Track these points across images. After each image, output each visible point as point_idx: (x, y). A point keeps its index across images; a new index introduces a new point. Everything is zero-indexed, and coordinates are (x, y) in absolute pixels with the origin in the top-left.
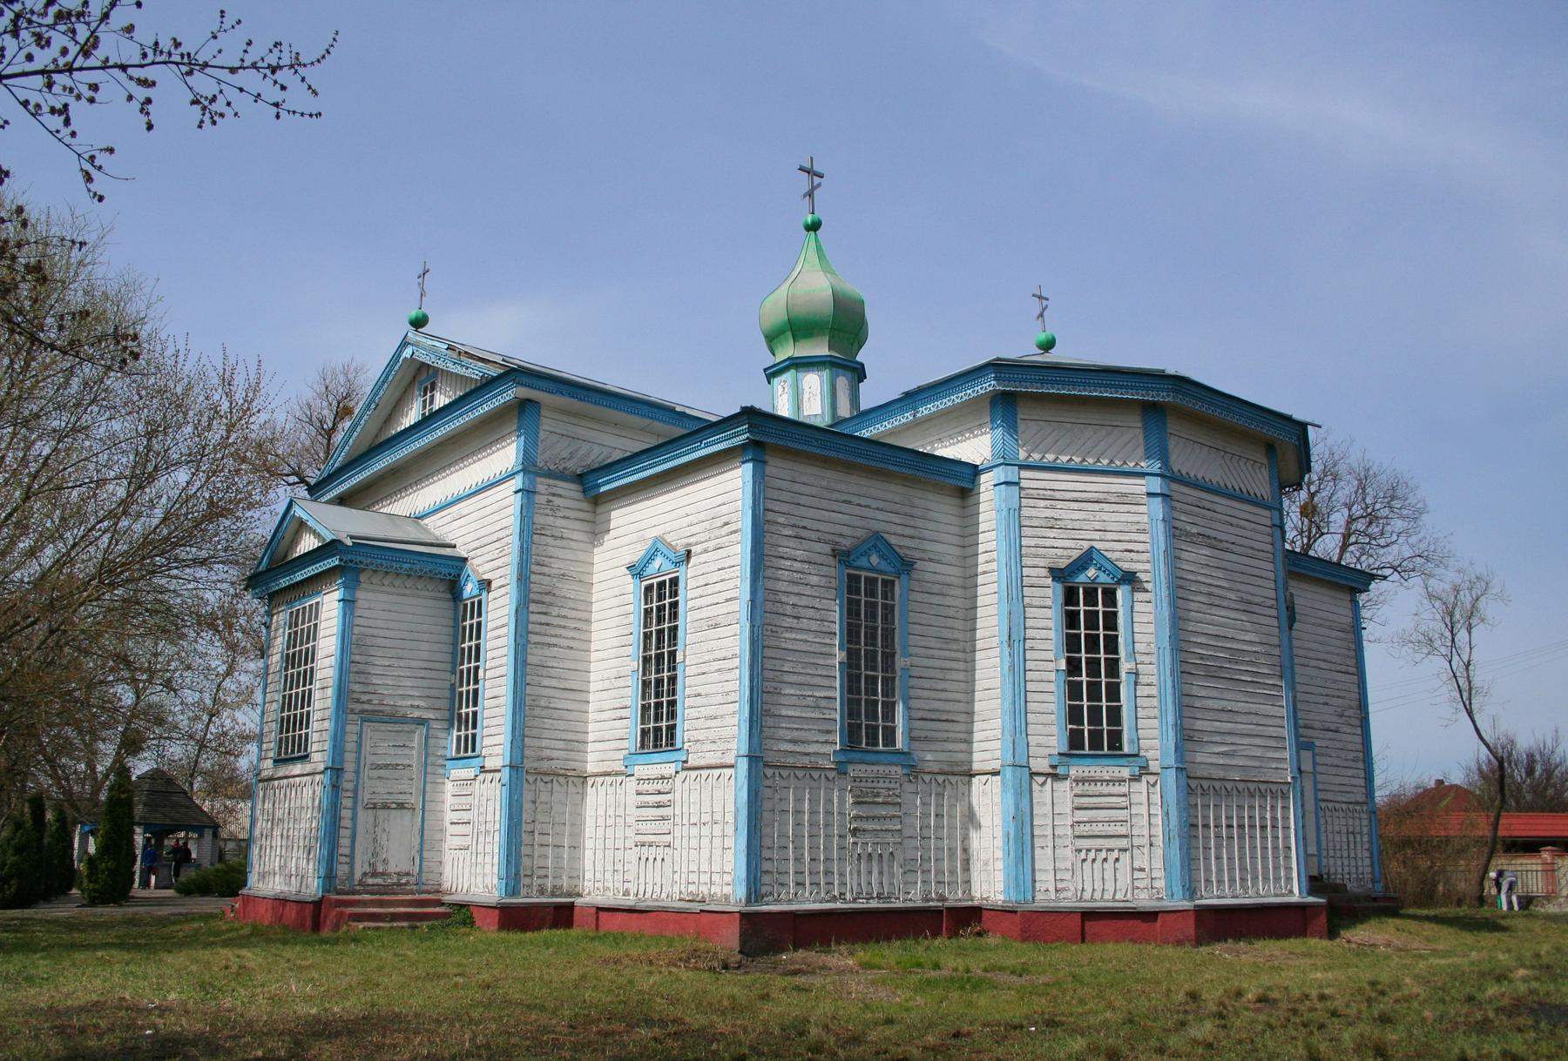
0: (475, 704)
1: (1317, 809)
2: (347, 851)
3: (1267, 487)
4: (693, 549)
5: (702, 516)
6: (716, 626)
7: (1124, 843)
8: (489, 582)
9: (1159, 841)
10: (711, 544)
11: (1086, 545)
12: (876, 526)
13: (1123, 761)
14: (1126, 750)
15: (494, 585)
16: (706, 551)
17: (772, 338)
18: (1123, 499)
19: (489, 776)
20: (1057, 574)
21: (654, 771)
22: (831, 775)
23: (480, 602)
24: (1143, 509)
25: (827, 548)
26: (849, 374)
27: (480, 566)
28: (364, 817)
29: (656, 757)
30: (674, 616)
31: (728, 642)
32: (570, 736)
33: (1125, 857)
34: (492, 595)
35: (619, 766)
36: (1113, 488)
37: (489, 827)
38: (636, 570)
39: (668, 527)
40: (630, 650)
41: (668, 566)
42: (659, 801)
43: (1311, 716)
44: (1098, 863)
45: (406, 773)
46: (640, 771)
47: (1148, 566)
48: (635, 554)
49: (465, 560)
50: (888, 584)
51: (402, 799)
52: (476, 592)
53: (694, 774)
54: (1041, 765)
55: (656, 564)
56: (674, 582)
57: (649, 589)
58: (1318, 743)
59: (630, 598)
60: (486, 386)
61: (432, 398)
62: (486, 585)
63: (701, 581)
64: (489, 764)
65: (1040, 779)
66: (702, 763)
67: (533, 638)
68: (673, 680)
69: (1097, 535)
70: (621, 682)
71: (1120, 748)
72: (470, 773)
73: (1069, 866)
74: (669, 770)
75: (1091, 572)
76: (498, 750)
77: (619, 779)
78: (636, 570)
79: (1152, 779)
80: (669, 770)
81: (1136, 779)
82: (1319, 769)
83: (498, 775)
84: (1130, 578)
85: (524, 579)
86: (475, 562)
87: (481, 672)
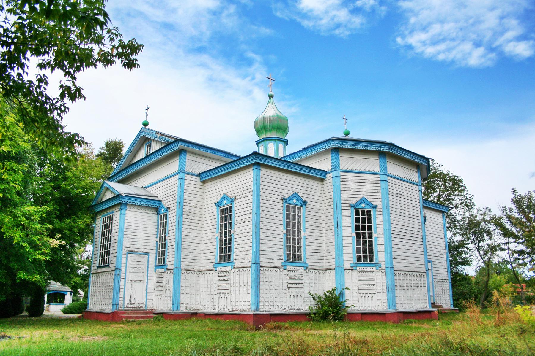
0: (165, 248)
1: (433, 282)
2: (122, 296)
3: (417, 178)
4: (237, 198)
5: (240, 187)
6: (245, 222)
7: (374, 291)
8: (169, 208)
9: (385, 291)
10: (243, 196)
11: (361, 196)
12: (295, 190)
13: (374, 265)
14: (375, 262)
15: (171, 209)
16: (241, 198)
17: (258, 132)
18: (373, 182)
19: (169, 271)
20: (352, 206)
21: (223, 269)
22: (281, 270)
23: (166, 215)
24: (379, 185)
25: (280, 197)
26: (283, 143)
27: (166, 203)
28: (128, 285)
29: (225, 265)
30: (230, 219)
31: (249, 227)
32: (196, 258)
33: (374, 296)
34: (170, 213)
35: (212, 268)
36: (370, 179)
37: (170, 288)
38: (218, 205)
39: (228, 190)
40: (215, 230)
41: (228, 203)
42: (225, 279)
43: (430, 252)
44: (363, 297)
45: (142, 271)
46: (219, 269)
47: (381, 203)
48: (217, 199)
49: (161, 201)
50: (299, 209)
51: (140, 279)
52: (165, 211)
53: (237, 270)
54: (347, 266)
55: (225, 202)
56: (231, 208)
57: (222, 210)
58: (432, 260)
59: (216, 213)
60: (169, 144)
61: (150, 149)
62: (168, 209)
63: (239, 208)
64: (169, 267)
65: (347, 271)
66: (240, 266)
67: (184, 226)
68: (230, 239)
69: (365, 193)
70: (213, 241)
71: (373, 261)
72: (163, 270)
73: (357, 299)
74: (229, 269)
75: (363, 205)
76: (172, 263)
77: (212, 272)
78: (218, 205)
79: (383, 271)
80: (229, 269)
81: (377, 270)
82: (433, 269)
83: (172, 271)
84: (375, 207)
85: (180, 206)
86: (165, 202)
87: (167, 237)
